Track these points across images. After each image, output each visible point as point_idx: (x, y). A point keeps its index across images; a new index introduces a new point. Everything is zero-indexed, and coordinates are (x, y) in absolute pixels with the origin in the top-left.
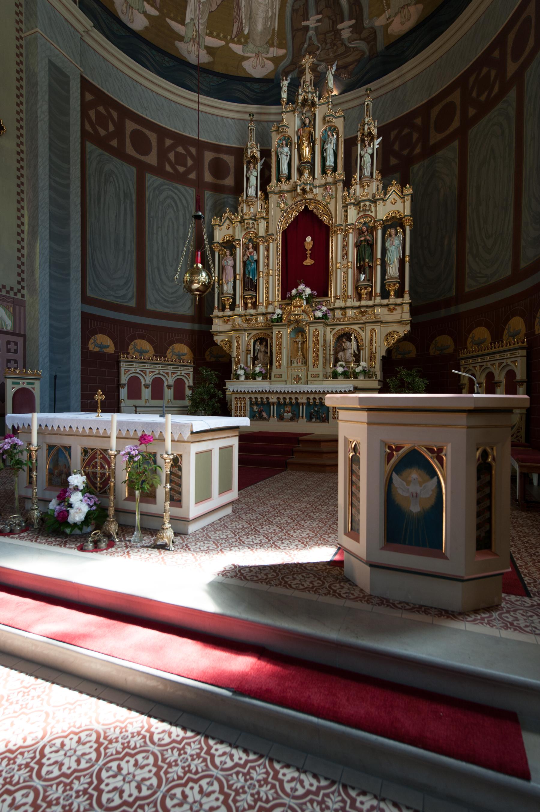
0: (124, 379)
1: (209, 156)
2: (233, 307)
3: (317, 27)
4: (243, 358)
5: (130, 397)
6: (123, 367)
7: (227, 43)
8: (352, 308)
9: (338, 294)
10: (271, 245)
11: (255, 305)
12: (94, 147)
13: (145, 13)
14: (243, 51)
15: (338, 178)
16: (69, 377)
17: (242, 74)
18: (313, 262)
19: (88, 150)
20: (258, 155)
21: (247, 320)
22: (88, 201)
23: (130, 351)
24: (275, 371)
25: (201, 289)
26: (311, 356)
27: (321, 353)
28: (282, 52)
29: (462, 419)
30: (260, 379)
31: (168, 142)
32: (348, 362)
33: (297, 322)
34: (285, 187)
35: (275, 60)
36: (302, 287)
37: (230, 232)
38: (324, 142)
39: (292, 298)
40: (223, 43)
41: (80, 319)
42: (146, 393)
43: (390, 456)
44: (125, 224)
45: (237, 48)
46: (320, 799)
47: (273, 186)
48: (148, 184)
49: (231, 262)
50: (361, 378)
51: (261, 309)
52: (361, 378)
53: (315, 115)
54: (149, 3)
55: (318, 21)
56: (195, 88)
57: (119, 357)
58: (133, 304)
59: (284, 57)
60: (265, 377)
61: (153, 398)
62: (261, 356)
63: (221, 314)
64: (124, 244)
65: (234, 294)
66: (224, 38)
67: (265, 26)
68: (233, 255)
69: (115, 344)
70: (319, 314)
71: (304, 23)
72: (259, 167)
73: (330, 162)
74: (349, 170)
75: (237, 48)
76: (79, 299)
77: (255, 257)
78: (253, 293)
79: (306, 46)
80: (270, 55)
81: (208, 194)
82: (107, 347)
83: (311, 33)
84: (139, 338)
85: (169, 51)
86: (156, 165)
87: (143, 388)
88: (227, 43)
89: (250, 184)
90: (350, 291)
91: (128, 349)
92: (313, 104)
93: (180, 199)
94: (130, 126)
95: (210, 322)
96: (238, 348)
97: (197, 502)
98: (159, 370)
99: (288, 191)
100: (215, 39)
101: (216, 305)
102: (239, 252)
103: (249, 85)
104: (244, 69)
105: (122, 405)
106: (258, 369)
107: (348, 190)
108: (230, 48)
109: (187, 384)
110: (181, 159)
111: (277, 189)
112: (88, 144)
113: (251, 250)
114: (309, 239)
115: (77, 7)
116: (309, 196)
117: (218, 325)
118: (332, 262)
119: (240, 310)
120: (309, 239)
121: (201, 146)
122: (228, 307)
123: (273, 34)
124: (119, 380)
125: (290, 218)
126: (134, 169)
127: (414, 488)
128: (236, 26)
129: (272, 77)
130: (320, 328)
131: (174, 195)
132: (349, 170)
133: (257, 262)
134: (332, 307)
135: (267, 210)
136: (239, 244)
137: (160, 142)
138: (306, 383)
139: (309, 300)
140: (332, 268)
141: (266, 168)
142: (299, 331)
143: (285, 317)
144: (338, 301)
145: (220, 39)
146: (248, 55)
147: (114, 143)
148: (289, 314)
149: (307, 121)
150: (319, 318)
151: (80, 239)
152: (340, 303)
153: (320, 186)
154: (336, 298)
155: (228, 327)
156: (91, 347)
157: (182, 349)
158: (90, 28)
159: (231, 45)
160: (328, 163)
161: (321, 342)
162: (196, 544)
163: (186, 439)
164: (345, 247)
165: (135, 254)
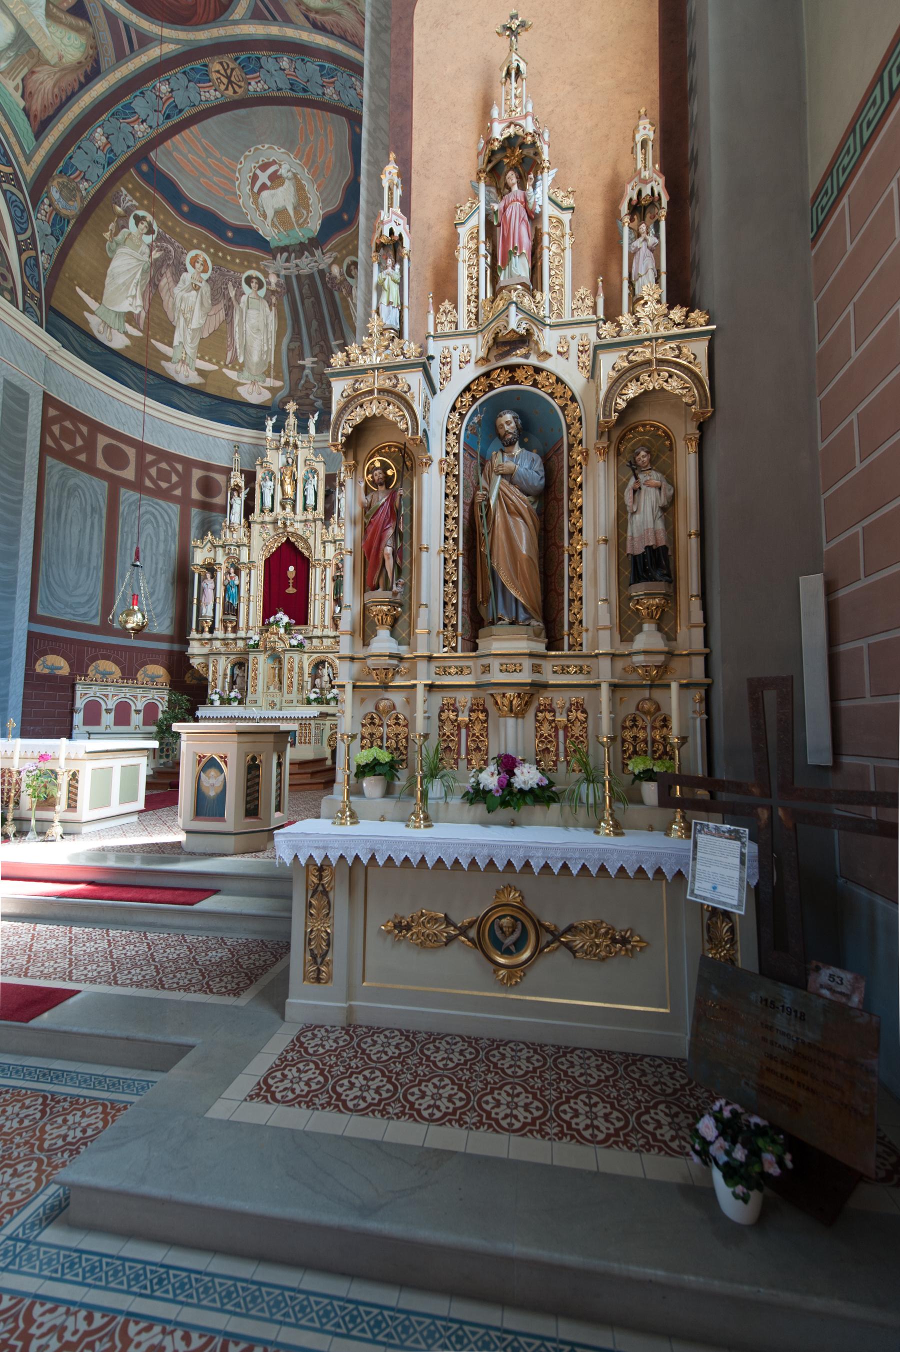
0: (80, 703)
1: (197, 474)
2: (212, 629)
3: (313, 368)
4: (220, 682)
5: (86, 723)
6: (79, 690)
7: (221, 368)
8: (328, 637)
9: (316, 624)
10: (253, 572)
11: (235, 629)
12: (55, 461)
13: (126, 333)
14: (238, 377)
15: (316, 517)
16: (7, 701)
17: (237, 398)
18: (295, 591)
19: (48, 465)
20: (242, 484)
21: (226, 645)
22: (44, 516)
23: (89, 672)
24: (250, 697)
25: (137, 628)
26: (286, 682)
27: (295, 680)
28: (279, 384)
29: (271, 738)
30: (236, 704)
31: (149, 458)
32: (322, 689)
33: (273, 649)
34: (268, 518)
35: (271, 389)
36: (280, 615)
37: (212, 554)
38: (306, 481)
39: (270, 624)
40: (216, 368)
41: (26, 639)
42: (107, 719)
43: (200, 762)
44: (91, 539)
45: (232, 374)
46: (537, 1128)
47: (256, 516)
48: (122, 498)
49: (212, 585)
50: (333, 703)
51: (241, 634)
52: (333, 703)
53: (297, 457)
54: (130, 325)
55: (313, 363)
56: (183, 406)
57: (74, 679)
58: (97, 622)
59: (281, 388)
60: (241, 702)
61: (116, 724)
62: (238, 681)
63: (198, 636)
64: (89, 560)
65: (214, 617)
66: (218, 363)
67: (261, 359)
68: (214, 577)
69: (71, 666)
70: (294, 642)
71: (300, 362)
72: (243, 495)
73: (311, 501)
74: (329, 512)
75: (232, 374)
76: (27, 618)
77: (237, 582)
78: (234, 618)
79: (302, 382)
80: (267, 385)
81: (194, 511)
82: (61, 668)
83: (307, 371)
84: (102, 659)
85: (153, 369)
86: (133, 479)
87: (104, 713)
88: (221, 368)
89: (233, 511)
90: (328, 621)
91: (87, 670)
92: (296, 446)
93: (160, 514)
94: (103, 441)
95: (187, 643)
96: (215, 673)
97: (91, 808)
98: (125, 694)
99: (270, 523)
100: (207, 363)
101: (194, 626)
102: (220, 576)
103: (245, 409)
104: (239, 394)
105: (75, 732)
106: (233, 694)
107: (327, 528)
108: (224, 374)
109: (161, 708)
110: (164, 475)
111: (260, 520)
112: (50, 461)
113: (233, 575)
114: (291, 568)
115: (43, 331)
116: (290, 529)
117: (195, 648)
118: (312, 592)
119: (219, 633)
120: (291, 568)
121: (189, 464)
122: (207, 629)
123: (270, 367)
124: (73, 704)
125: (272, 548)
126: (106, 484)
127: (212, 781)
128: (229, 354)
129: (269, 404)
130: (296, 656)
131: (154, 510)
132: (329, 512)
133: (238, 586)
134: (310, 635)
135: (249, 537)
136: (220, 568)
137: (140, 458)
138: (281, 709)
139: (287, 627)
140: (311, 598)
141: (250, 497)
142: (276, 658)
143: (261, 643)
144: (315, 630)
145: (213, 363)
146: (244, 381)
147: (82, 457)
148: (266, 639)
149: (290, 461)
150: (294, 646)
151: (31, 555)
152: (318, 632)
153: (301, 522)
154: (314, 626)
155: (206, 650)
156: (39, 668)
157: (158, 671)
158: (57, 348)
159: (225, 370)
160: (308, 502)
161: (296, 669)
162: (265, 961)
163: (80, 757)
164: (323, 580)
165: (102, 570)
